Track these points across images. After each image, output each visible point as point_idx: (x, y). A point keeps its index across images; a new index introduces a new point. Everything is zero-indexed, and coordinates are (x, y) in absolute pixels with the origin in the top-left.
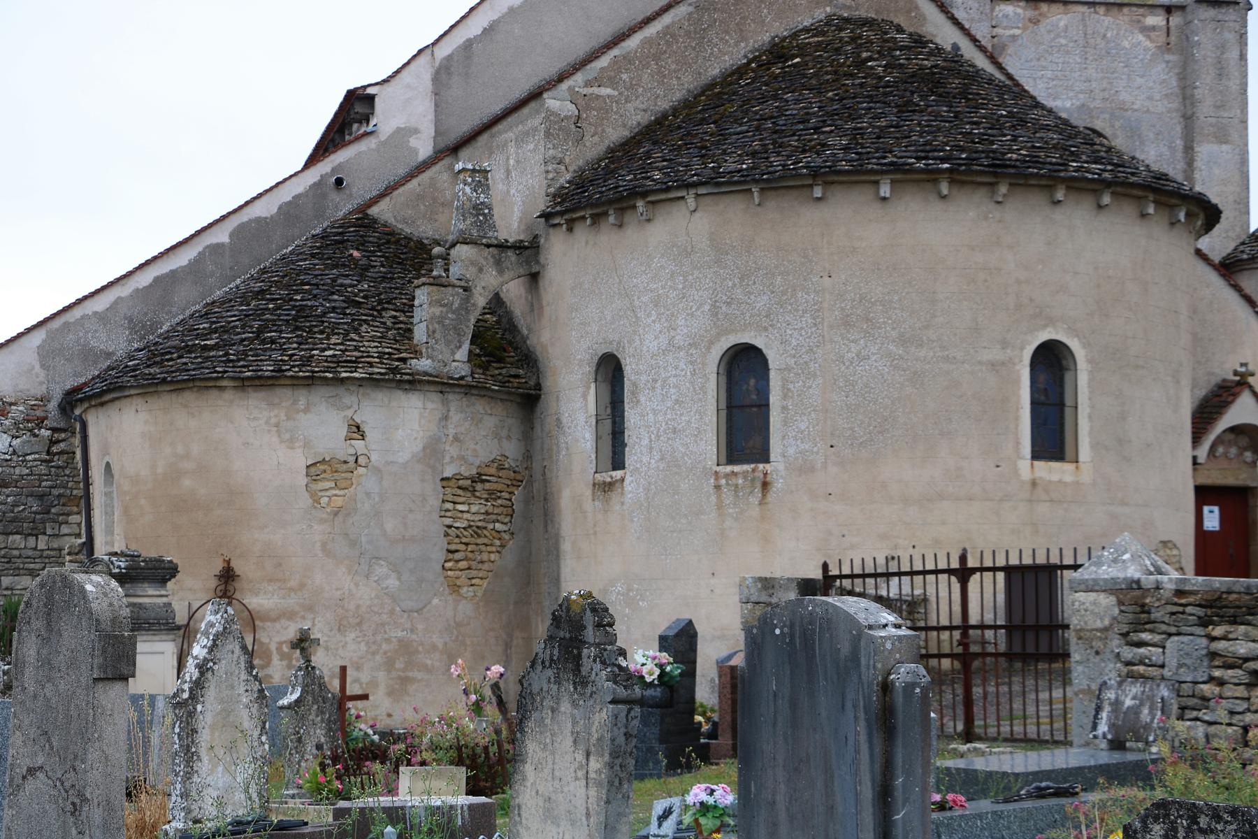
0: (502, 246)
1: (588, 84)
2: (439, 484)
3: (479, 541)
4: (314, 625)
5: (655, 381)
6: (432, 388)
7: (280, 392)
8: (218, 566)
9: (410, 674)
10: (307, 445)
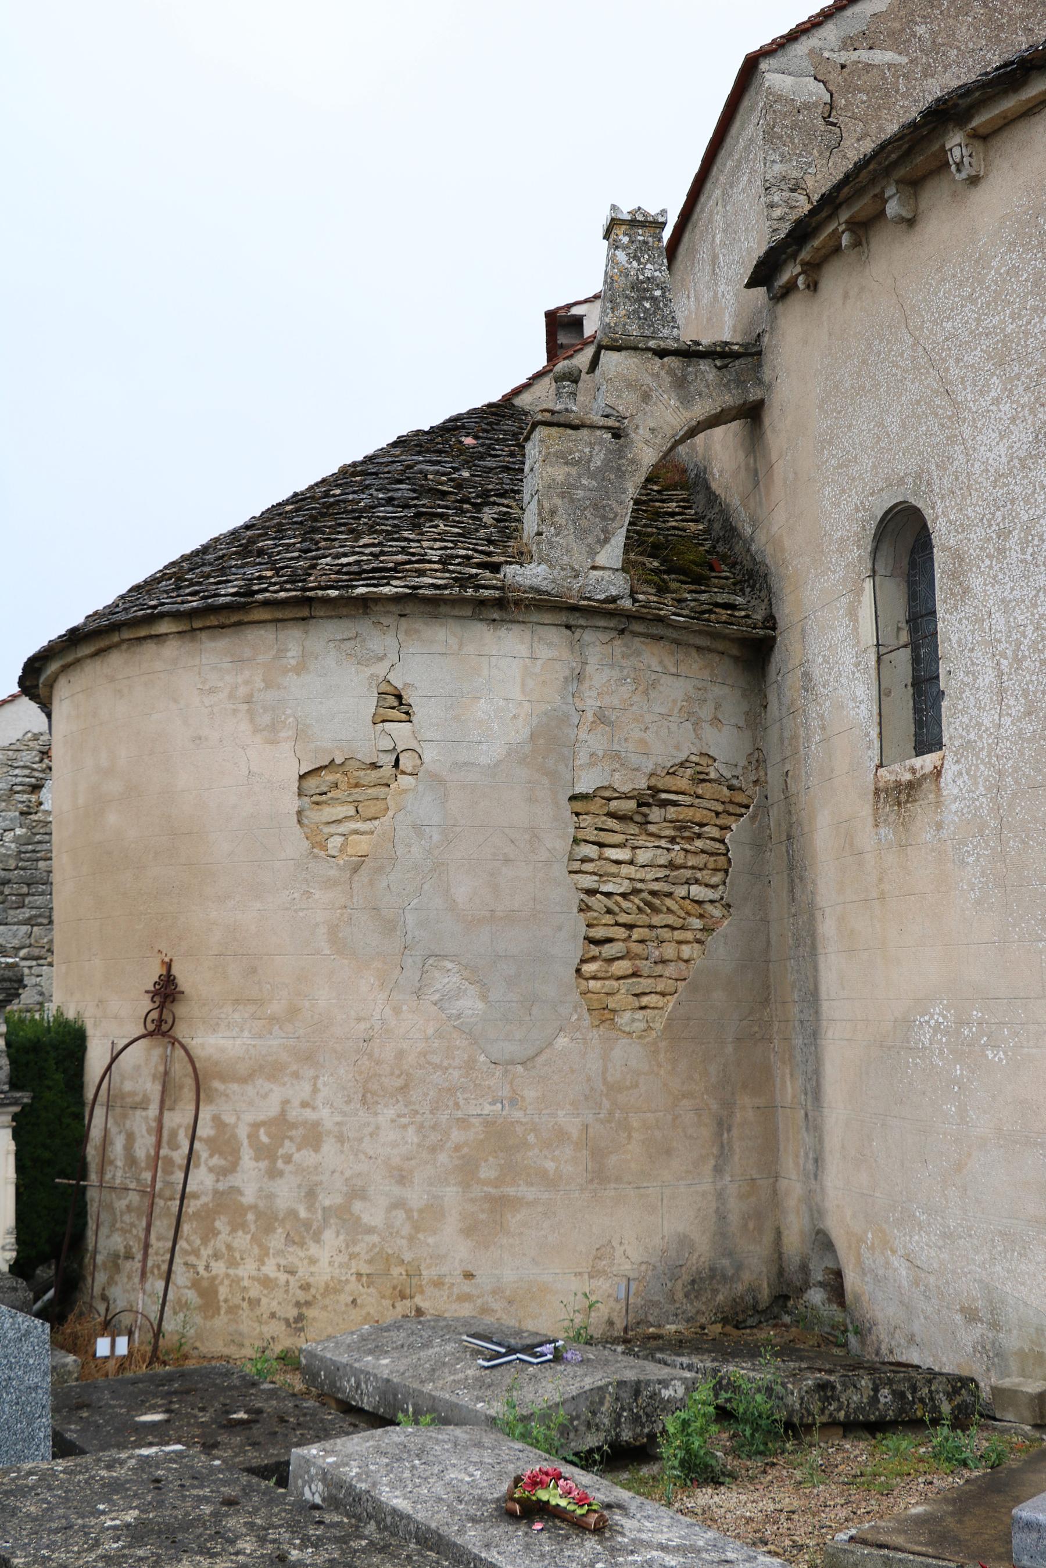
0: (690, 353)
1: (849, 43)
2: (567, 808)
3: (656, 920)
4: (315, 1090)
5: (1004, 534)
6: (547, 618)
7: (253, 635)
8: (155, 972)
9: (511, 1191)
10: (301, 734)
